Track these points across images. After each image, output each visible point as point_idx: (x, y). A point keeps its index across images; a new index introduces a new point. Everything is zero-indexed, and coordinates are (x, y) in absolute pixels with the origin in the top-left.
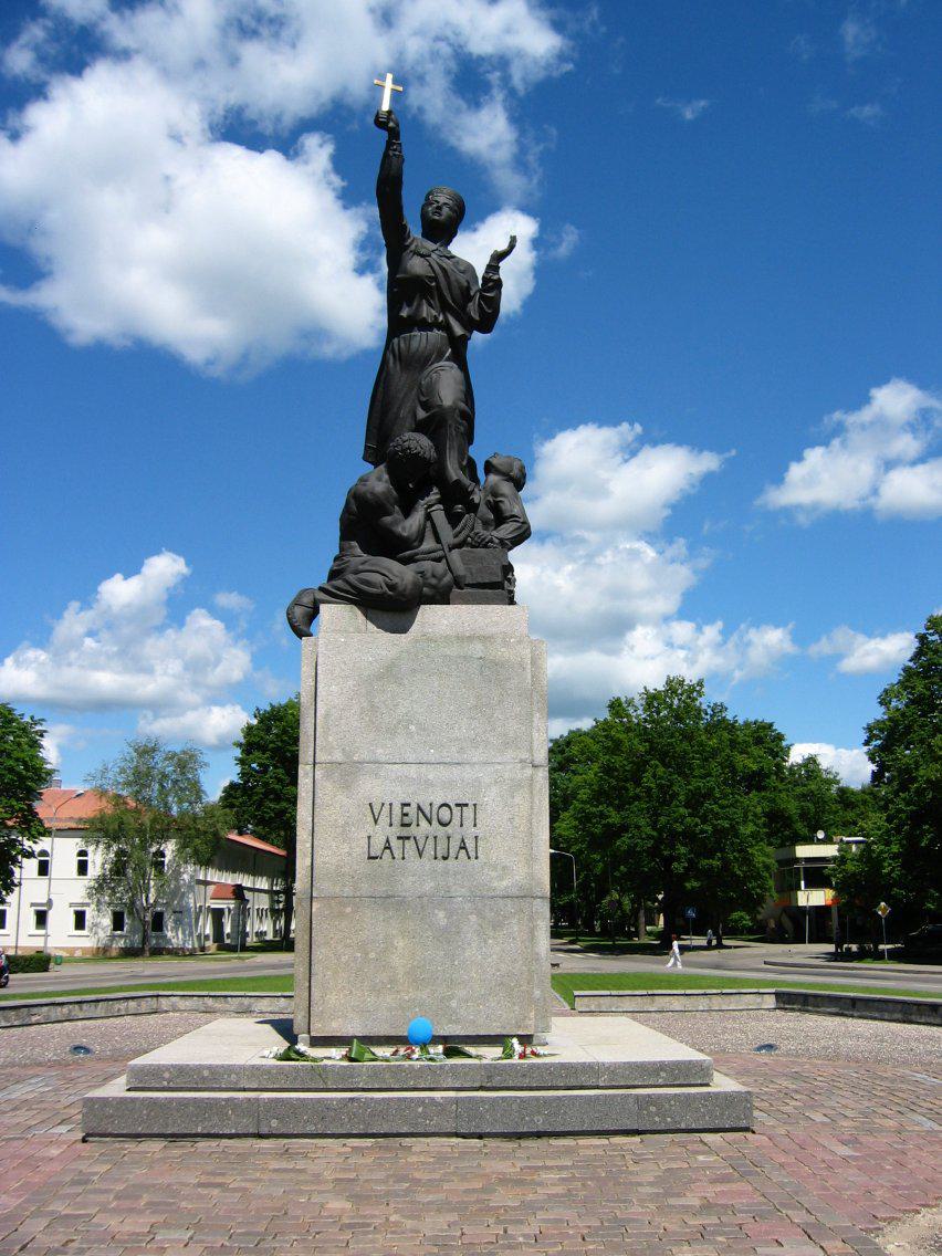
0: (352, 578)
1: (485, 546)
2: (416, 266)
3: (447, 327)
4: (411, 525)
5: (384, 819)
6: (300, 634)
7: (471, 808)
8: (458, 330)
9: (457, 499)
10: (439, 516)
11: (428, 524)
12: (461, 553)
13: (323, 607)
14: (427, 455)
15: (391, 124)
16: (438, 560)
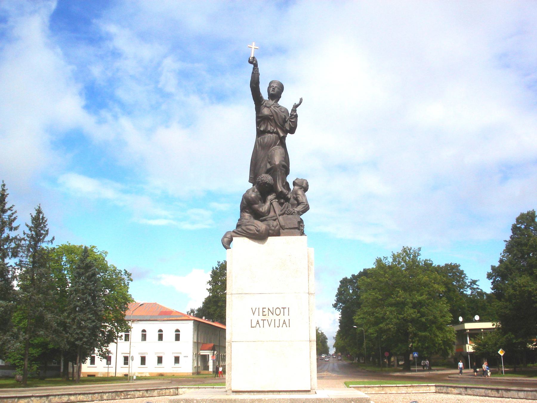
0: (244, 228)
1: (292, 214)
2: (266, 111)
3: (277, 133)
4: (265, 208)
6: (226, 248)
7: (287, 309)
8: (282, 135)
9: (282, 198)
10: (275, 204)
11: (272, 207)
12: (283, 218)
13: (234, 238)
14: (270, 183)
15: (254, 62)
16: (275, 220)
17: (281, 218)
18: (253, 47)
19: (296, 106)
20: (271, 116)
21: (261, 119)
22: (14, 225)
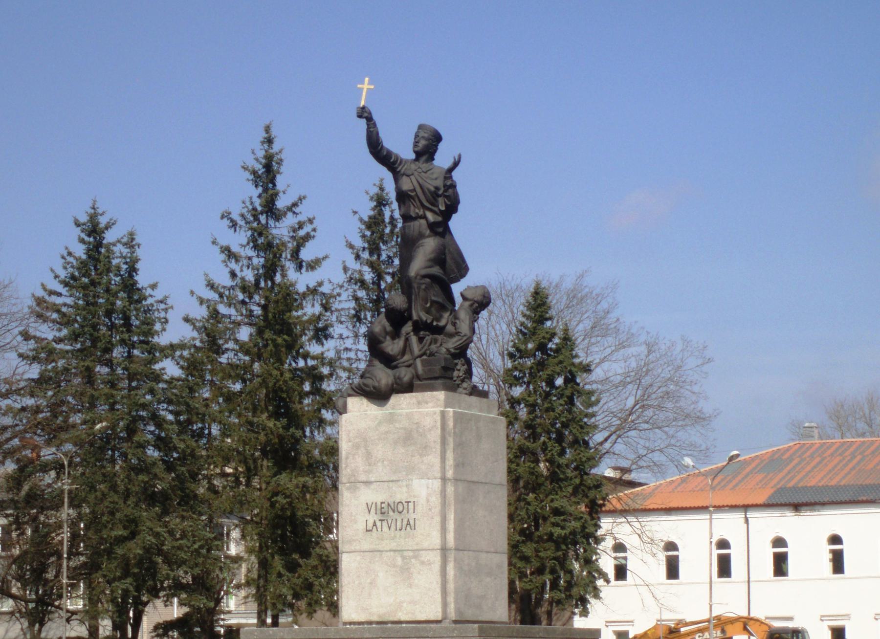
5: (373, 510)
10: (414, 339)
16: (409, 366)
20: (411, 191)
22: (306, 254)
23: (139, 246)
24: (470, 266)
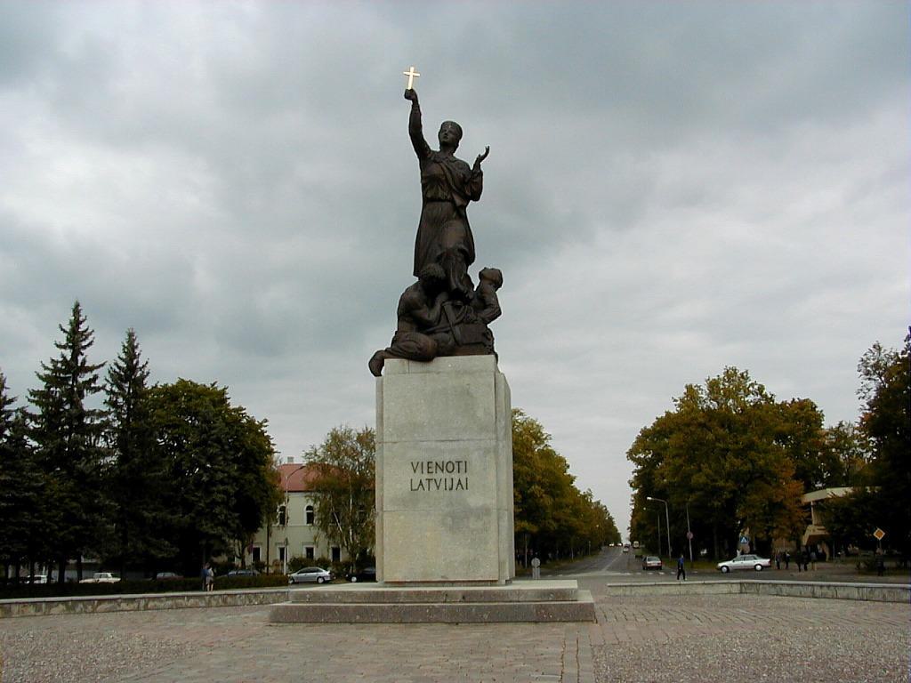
1: (473, 323)
2: (435, 169)
3: (452, 201)
8: (458, 201)
10: (448, 306)
17: (457, 330)
18: (411, 74)
19: (480, 159)
21: (428, 182)
23: (568, 467)
24: (801, 396)
